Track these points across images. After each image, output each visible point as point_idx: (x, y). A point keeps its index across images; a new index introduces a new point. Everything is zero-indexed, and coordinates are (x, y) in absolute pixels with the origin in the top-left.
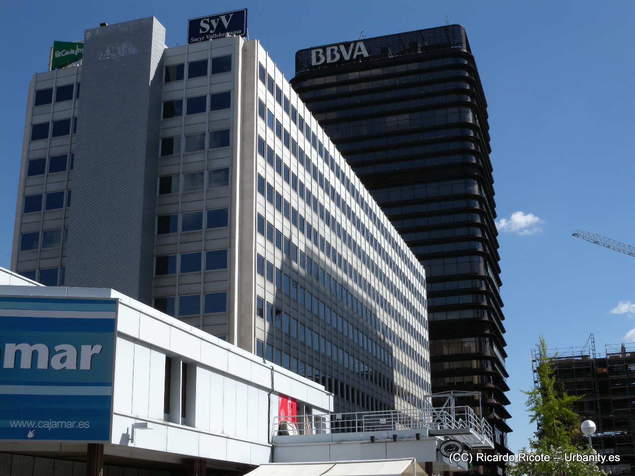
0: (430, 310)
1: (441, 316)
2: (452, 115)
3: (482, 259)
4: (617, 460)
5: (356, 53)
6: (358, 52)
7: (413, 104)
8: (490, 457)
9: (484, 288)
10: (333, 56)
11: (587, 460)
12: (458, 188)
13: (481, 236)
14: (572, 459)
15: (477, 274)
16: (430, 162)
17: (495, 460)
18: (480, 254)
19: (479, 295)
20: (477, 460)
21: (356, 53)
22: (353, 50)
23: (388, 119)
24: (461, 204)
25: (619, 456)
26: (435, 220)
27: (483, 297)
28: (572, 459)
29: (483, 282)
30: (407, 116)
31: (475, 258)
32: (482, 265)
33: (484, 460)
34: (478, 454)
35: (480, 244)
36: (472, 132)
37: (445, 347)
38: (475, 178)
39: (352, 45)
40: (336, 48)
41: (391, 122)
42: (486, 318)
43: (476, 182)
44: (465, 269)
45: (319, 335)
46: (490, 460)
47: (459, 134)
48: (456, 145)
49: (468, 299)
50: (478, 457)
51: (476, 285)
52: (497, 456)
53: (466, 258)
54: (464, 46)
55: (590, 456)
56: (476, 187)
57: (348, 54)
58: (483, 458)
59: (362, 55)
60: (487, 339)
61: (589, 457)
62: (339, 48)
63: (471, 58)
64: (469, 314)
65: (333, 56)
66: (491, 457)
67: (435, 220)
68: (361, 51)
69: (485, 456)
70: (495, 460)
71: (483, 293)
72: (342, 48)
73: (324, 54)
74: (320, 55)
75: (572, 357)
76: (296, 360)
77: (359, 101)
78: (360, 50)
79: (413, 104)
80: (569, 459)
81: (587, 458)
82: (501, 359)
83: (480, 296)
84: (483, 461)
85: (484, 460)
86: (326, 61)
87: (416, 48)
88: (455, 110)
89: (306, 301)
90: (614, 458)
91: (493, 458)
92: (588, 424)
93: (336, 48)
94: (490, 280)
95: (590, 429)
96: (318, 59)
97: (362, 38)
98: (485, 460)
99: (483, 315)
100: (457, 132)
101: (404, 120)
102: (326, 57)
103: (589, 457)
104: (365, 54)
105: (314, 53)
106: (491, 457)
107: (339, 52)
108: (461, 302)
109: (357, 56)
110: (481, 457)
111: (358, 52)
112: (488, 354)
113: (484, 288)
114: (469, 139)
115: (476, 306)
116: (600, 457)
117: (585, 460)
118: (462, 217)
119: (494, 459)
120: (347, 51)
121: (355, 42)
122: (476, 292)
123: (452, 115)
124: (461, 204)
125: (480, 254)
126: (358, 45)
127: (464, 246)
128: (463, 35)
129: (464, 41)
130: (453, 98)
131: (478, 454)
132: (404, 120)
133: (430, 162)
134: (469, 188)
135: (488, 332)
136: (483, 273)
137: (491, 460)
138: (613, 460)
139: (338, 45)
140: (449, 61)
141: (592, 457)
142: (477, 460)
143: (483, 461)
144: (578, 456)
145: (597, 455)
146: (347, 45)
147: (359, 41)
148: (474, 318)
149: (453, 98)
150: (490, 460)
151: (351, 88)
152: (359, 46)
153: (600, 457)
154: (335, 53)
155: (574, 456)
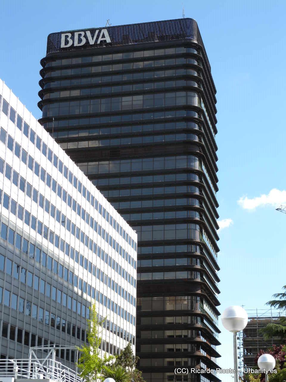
0: (140, 270)
1: (147, 277)
2: (180, 99)
3: (198, 227)
4: (275, 370)
5: (100, 39)
6: (102, 38)
7: (147, 87)
8: (199, 371)
9: (198, 253)
10: (80, 41)
11: (257, 372)
12: (181, 163)
13: (199, 194)
14: (248, 372)
15: (192, 239)
16: (159, 139)
17: (202, 372)
18: (196, 222)
19: (194, 259)
20: (191, 373)
21: (100, 39)
22: (97, 36)
23: (125, 99)
24: (182, 177)
25: (276, 370)
26: (158, 191)
27: (197, 260)
28: (248, 372)
29: (198, 247)
30: (140, 97)
31: (192, 226)
32: (198, 233)
33: (195, 372)
34: (192, 369)
35: (197, 213)
36: (197, 137)
37: (168, 304)
38: (196, 155)
39: (97, 32)
40: (83, 33)
41: (127, 102)
42: (199, 280)
43: (197, 159)
44: (182, 235)
45: (18, 296)
46: (199, 372)
47: (185, 116)
48: (181, 125)
49: (183, 262)
50: (192, 371)
51: (192, 250)
52: (203, 370)
53: (184, 226)
54: (195, 38)
55: (259, 370)
56: (197, 163)
57: (93, 39)
58: (195, 371)
59: (105, 41)
60: (198, 298)
61: (258, 371)
62: (85, 34)
63: (200, 48)
64: (183, 275)
65: (80, 41)
66: (200, 370)
67: (158, 191)
68: (104, 37)
69: (196, 370)
70: (202, 372)
71: (197, 257)
72: (88, 34)
73: (73, 38)
74: (69, 39)
75: (270, 318)
76: (85, 307)
77: (100, 82)
78: (103, 36)
79: (147, 87)
80: (246, 372)
81: (257, 371)
82: (214, 134)
83: (194, 259)
84: (195, 373)
85: (195, 372)
86: (73, 44)
87: (153, 37)
88: (183, 94)
89: (47, 262)
90: (273, 371)
91: (200, 371)
92: (265, 359)
93: (83, 33)
94: (205, 246)
95: (267, 365)
96: (67, 42)
97: (108, 26)
98: (196, 373)
99: (196, 277)
100: (183, 114)
101: (138, 101)
102: (73, 41)
103: (258, 371)
104: (108, 40)
105: (63, 36)
106: (200, 370)
107: (85, 36)
108: (177, 265)
109: (101, 41)
110: (193, 371)
111: (102, 38)
112: (199, 311)
113: (198, 253)
114: (193, 120)
115: (190, 269)
116: (265, 371)
117: (256, 372)
118: (182, 190)
119: (201, 372)
120: (93, 37)
121: (100, 29)
122: (190, 256)
123: (180, 99)
124: (182, 177)
125: (196, 222)
126: (103, 31)
127: (182, 214)
128: (195, 27)
129: (196, 33)
130: (182, 83)
131: (192, 369)
132: (138, 101)
133: (159, 139)
134: (192, 164)
135: (199, 292)
136: (198, 240)
137: (200, 372)
138: (273, 372)
139: (85, 31)
140: (182, 50)
141: (260, 371)
142: (191, 373)
143: (195, 373)
144: (252, 370)
145: (263, 369)
146: (93, 31)
147: (104, 28)
148: (188, 279)
149: (182, 83)
150: (199, 372)
151: (94, 70)
152: (103, 34)
153: (265, 371)
154: (82, 37)
155: (249, 370)
